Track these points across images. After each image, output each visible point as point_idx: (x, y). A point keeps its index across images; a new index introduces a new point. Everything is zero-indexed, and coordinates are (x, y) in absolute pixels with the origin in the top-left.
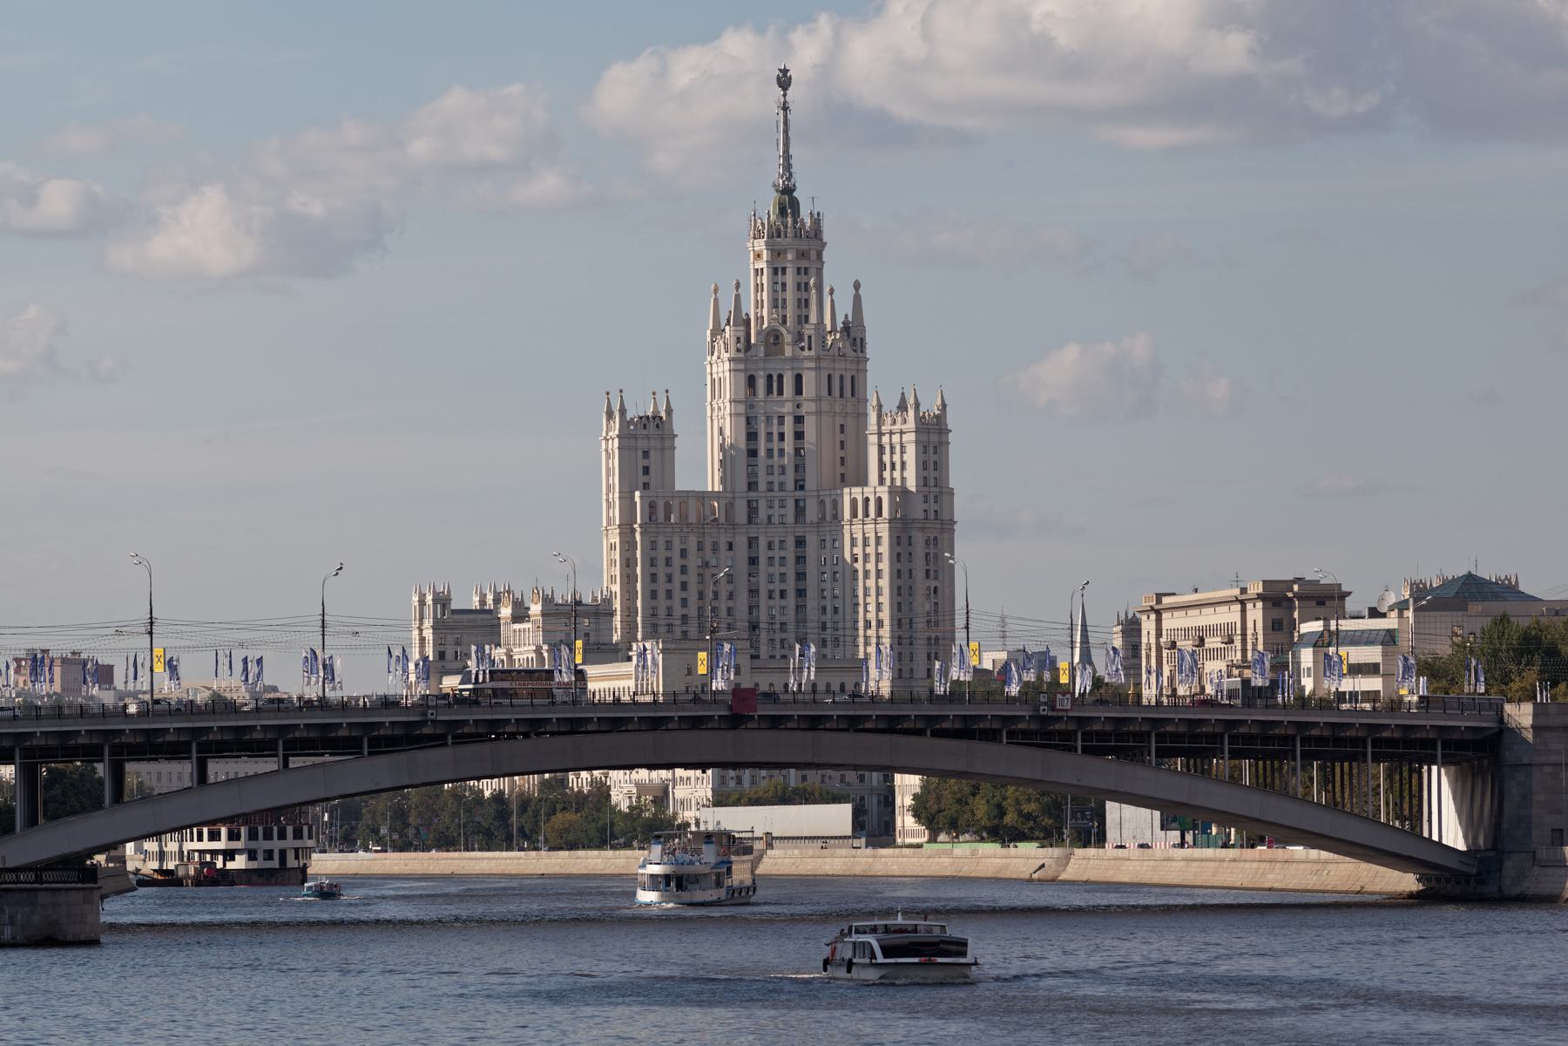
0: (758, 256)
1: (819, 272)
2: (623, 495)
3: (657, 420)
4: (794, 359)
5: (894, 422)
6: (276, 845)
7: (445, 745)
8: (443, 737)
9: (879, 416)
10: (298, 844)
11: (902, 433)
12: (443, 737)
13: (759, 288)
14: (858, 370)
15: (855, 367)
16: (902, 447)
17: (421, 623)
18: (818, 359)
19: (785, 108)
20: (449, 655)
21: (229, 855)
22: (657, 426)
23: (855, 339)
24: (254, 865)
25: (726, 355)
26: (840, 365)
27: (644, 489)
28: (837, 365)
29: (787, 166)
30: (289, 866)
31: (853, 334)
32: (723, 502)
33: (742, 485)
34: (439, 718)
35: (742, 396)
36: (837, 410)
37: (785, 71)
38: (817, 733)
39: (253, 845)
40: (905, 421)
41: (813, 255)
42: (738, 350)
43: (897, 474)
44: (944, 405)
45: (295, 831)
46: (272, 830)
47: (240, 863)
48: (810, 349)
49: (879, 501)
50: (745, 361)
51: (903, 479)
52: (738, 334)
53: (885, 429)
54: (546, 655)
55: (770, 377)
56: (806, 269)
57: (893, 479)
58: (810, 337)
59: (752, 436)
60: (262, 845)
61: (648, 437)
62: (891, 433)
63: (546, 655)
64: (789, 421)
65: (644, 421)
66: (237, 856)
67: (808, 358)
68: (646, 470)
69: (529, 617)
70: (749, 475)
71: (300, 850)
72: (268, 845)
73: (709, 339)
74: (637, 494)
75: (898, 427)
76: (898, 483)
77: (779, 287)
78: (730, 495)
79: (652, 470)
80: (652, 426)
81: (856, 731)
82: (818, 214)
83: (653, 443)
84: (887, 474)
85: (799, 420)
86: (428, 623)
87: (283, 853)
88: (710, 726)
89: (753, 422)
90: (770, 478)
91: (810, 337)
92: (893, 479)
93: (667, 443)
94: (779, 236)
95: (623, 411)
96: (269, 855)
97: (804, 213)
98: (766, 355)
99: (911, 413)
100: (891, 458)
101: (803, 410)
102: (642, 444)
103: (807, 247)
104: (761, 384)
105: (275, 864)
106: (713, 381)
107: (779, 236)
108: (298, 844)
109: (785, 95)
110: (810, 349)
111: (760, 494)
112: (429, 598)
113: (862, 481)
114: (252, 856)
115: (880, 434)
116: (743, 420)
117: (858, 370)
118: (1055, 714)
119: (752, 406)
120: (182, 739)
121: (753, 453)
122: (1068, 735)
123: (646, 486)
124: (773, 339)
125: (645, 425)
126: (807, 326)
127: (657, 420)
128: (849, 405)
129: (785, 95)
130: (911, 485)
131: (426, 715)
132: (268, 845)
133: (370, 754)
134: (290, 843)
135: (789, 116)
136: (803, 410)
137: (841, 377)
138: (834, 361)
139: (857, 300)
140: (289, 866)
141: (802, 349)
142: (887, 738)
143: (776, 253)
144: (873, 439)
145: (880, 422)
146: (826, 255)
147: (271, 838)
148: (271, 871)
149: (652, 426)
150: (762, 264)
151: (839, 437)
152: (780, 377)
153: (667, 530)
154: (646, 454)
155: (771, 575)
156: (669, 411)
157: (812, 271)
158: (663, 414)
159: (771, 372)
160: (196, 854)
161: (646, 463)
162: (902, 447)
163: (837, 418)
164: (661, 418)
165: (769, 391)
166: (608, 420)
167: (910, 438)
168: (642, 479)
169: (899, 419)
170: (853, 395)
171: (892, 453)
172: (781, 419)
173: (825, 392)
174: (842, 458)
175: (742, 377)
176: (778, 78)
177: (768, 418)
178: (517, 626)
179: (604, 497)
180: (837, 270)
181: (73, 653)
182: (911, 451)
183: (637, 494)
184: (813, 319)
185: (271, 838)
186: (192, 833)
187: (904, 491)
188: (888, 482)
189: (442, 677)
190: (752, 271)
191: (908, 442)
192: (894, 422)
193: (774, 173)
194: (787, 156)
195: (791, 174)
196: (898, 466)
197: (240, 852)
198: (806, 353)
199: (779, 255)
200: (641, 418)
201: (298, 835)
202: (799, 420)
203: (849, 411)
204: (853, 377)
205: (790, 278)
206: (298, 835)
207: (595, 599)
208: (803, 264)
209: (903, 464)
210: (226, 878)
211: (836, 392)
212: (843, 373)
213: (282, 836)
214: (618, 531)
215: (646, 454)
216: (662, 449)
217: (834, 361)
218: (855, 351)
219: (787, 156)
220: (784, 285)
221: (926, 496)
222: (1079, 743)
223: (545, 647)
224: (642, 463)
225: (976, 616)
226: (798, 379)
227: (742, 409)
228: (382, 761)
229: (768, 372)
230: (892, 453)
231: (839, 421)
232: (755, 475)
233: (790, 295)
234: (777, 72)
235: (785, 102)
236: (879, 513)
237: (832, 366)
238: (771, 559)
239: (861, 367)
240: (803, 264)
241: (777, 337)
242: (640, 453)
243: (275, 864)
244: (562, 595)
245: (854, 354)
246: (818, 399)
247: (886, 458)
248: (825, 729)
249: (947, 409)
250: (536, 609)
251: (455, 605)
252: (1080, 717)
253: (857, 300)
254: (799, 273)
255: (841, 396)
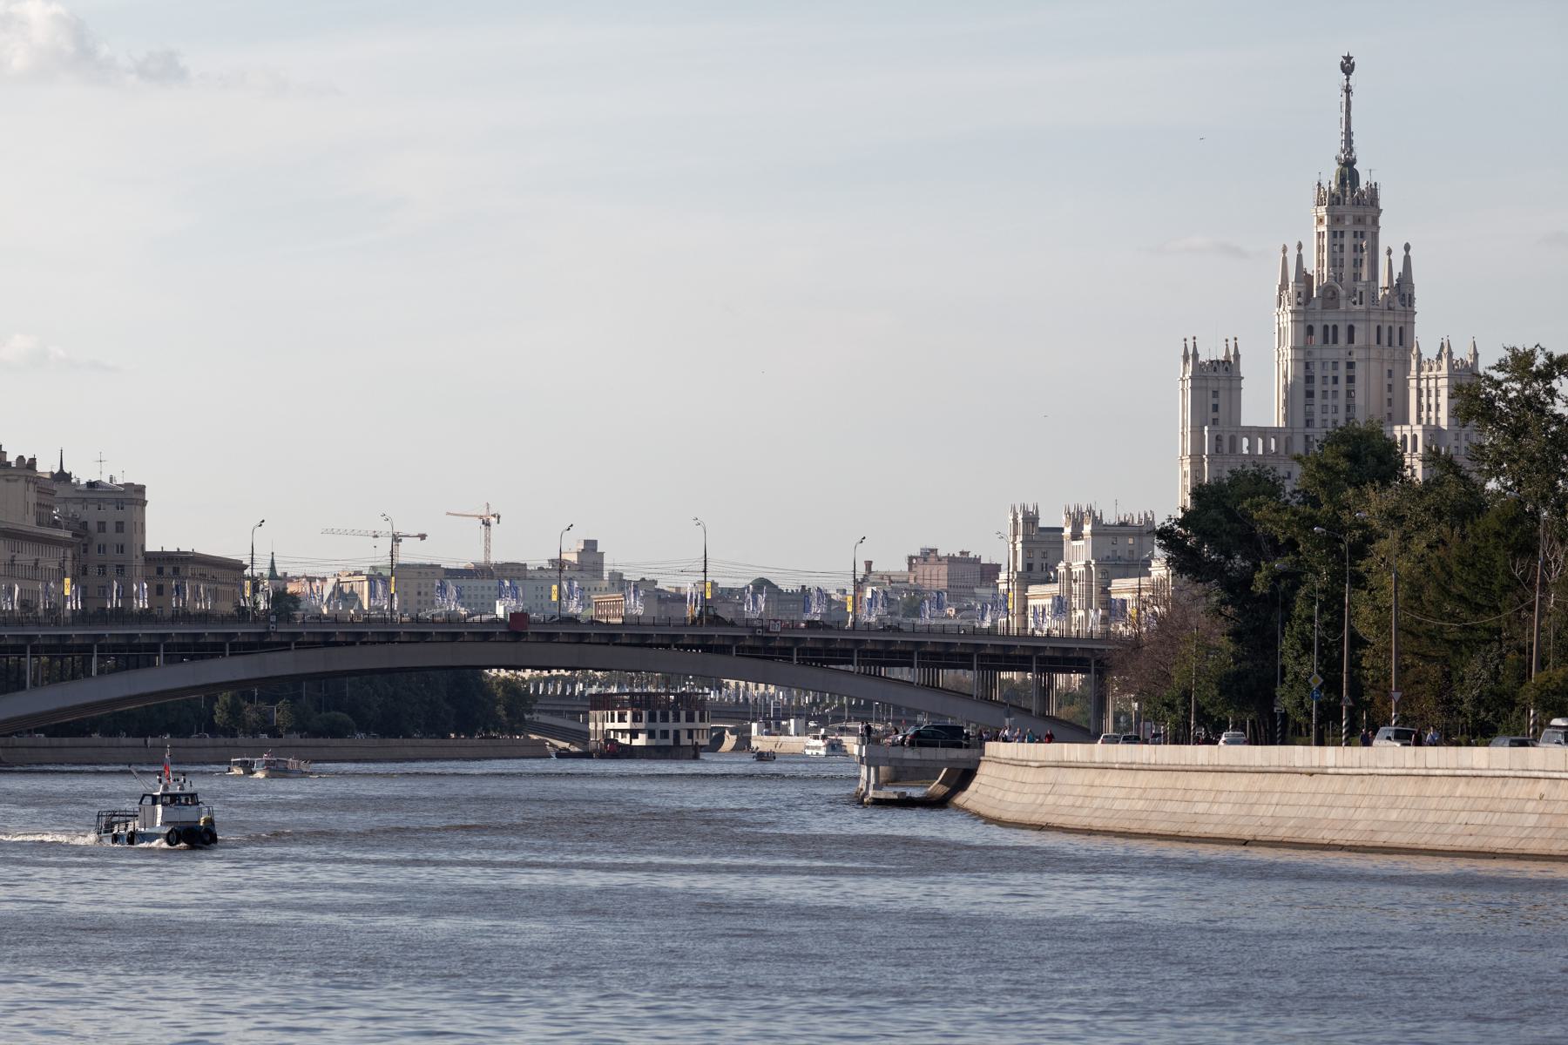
0: (1321, 221)
1: (1375, 236)
2: (1195, 429)
3: (1227, 365)
4: (1347, 312)
5: (1431, 369)
6: (671, 726)
7: (289, 649)
8: (288, 644)
9: (1419, 363)
10: (690, 725)
11: (1437, 378)
12: (288, 644)
13: (1320, 249)
14: (1406, 322)
15: (1403, 319)
16: (1437, 391)
17: (1015, 539)
18: (1368, 312)
19: (1348, 90)
20: (1036, 567)
21: (634, 734)
22: (1227, 369)
23: (1404, 295)
24: (653, 742)
25: (1290, 308)
26: (1389, 318)
27: (1214, 424)
28: (1386, 318)
29: (1349, 141)
30: (682, 743)
31: (1403, 291)
32: (1283, 438)
33: (1300, 421)
34: (279, 630)
35: (1301, 344)
36: (1386, 357)
37: (1348, 58)
38: (455, 644)
39: (652, 726)
40: (1439, 368)
41: (1369, 220)
42: (1299, 304)
43: (1432, 414)
44: (1476, 355)
45: (619, 715)
46: (655, 715)
47: (641, 740)
48: (1361, 303)
49: (1415, 438)
50: (1306, 312)
51: (1437, 419)
52: (1299, 290)
53: (1423, 374)
54: (1093, 569)
55: (1326, 327)
56: (1362, 233)
57: (1429, 419)
58: (1361, 293)
59: (1309, 379)
60: (659, 726)
61: (1217, 379)
62: (1428, 378)
63: (1093, 569)
64: (1342, 367)
65: (1215, 364)
66: (640, 735)
67: (1360, 311)
68: (1216, 408)
69: (1082, 535)
70: (1307, 414)
71: (695, 732)
72: (664, 726)
73: (1277, 294)
74: (1206, 428)
75: (1434, 372)
76: (1433, 423)
77: (1337, 248)
78: (1289, 430)
79: (1221, 408)
80: (1221, 369)
81: (615, 644)
82: (1376, 184)
83: (1222, 384)
84: (1424, 415)
85: (1350, 365)
86: (1020, 538)
87: (677, 733)
88: (429, 639)
89: (1311, 367)
90: (1325, 416)
91: (1361, 293)
92: (1429, 419)
93: (1234, 384)
94: (1339, 204)
95: (1196, 355)
96: (665, 734)
97: (1363, 186)
98: (1323, 308)
99: (1445, 360)
100: (1428, 400)
101: (1354, 357)
102: (1212, 385)
103: (1362, 214)
104: (1318, 331)
105: (670, 742)
106: (1280, 329)
107: (1339, 204)
108: (690, 725)
109: (1348, 79)
110: (1361, 303)
111: (1315, 430)
112: (1020, 517)
113: (1405, 421)
114: (651, 735)
115: (1419, 379)
116: (1302, 366)
117: (1406, 322)
118: (769, 635)
119: (1309, 353)
120: (87, 642)
121: (1310, 394)
122: (787, 651)
123: (1215, 422)
124: (1330, 296)
125: (1227, 369)
126: (1359, 283)
127: (1227, 365)
128: (1397, 353)
129: (1348, 79)
130: (1444, 424)
131: (268, 628)
132: (664, 726)
133: (230, 655)
134: (683, 725)
135: (1351, 98)
136: (1354, 357)
137: (1390, 328)
138: (1383, 314)
139: (1407, 260)
140: (682, 743)
141: (1355, 303)
142: (637, 650)
143: (1335, 219)
144: (1413, 383)
145: (1420, 369)
146: (1382, 220)
147: (667, 721)
148: (667, 748)
149: (1221, 369)
150: (1323, 228)
151: (1387, 381)
152: (1335, 327)
153: (1231, 460)
154: (1215, 394)
155: (1326, 391)
156: (1237, 356)
157: (1368, 235)
158: (1232, 360)
159: (1328, 323)
160: (612, 733)
161: (1215, 401)
162: (1437, 391)
163: (1385, 364)
164: (1230, 362)
165: (1326, 341)
166: (1185, 364)
167: (1443, 382)
168: (1212, 415)
169: (1435, 367)
170: (1401, 344)
171: (1429, 396)
172: (1335, 363)
173: (1374, 340)
174: (1390, 400)
175: (1302, 327)
176: (1342, 64)
177: (1324, 364)
178: (1075, 543)
179: (1181, 431)
180: (1390, 236)
181: (962, 553)
182: (1444, 393)
183: (1206, 428)
184: (1365, 277)
185: (667, 721)
186: (613, 715)
187: (1438, 429)
188: (1424, 422)
189: (1027, 586)
190: (1315, 235)
191: (1442, 387)
192: (1431, 369)
193: (1336, 146)
194: (1348, 133)
195: (1352, 150)
196: (1433, 408)
197: (641, 731)
198: (1358, 307)
199: (1338, 220)
200: (1212, 362)
201: (690, 719)
202: (1350, 365)
203: (1397, 358)
204: (1401, 329)
205: (1348, 241)
206: (690, 719)
207: (1140, 522)
208: (1359, 228)
209: (1438, 406)
210: (629, 753)
211: (1385, 341)
212: (1392, 324)
213: (677, 719)
214: (1189, 461)
215: (1215, 394)
216: (1230, 389)
217: (1383, 314)
218: (1404, 305)
219: (1348, 133)
220: (1342, 246)
221: (1457, 434)
222: (795, 657)
223: (1093, 562)
224: (1212, 401)
225: (281, 565)
226: (1351, 329)
227: (1301, 355)
228: (238, 660)
229: (1324, 323)
230: (1429, 396)
231: (1387, 367)
232: (1312, 413)
233: (1348, 255)
234: (1342, 59)
235: (1348, 85)
236: (1415, 449)
237: (1381, 318)
238: (1325, 392)
239: (1408, 319)
240: (1359, 228)
241: (1334, 293)
242: (1210, 393)
243: (670, 742)
244: (1110, 518)
245: (1403, 308)
246: (1368, 347)
247: (1424, 400)
248: (589, 643)
249: (1480, 358)
250: (1087, 529)
251: (1042, 524)
252: (61, 635)
253: (1407, 260)
254: (1355, 236)
255: (1390, 344)
